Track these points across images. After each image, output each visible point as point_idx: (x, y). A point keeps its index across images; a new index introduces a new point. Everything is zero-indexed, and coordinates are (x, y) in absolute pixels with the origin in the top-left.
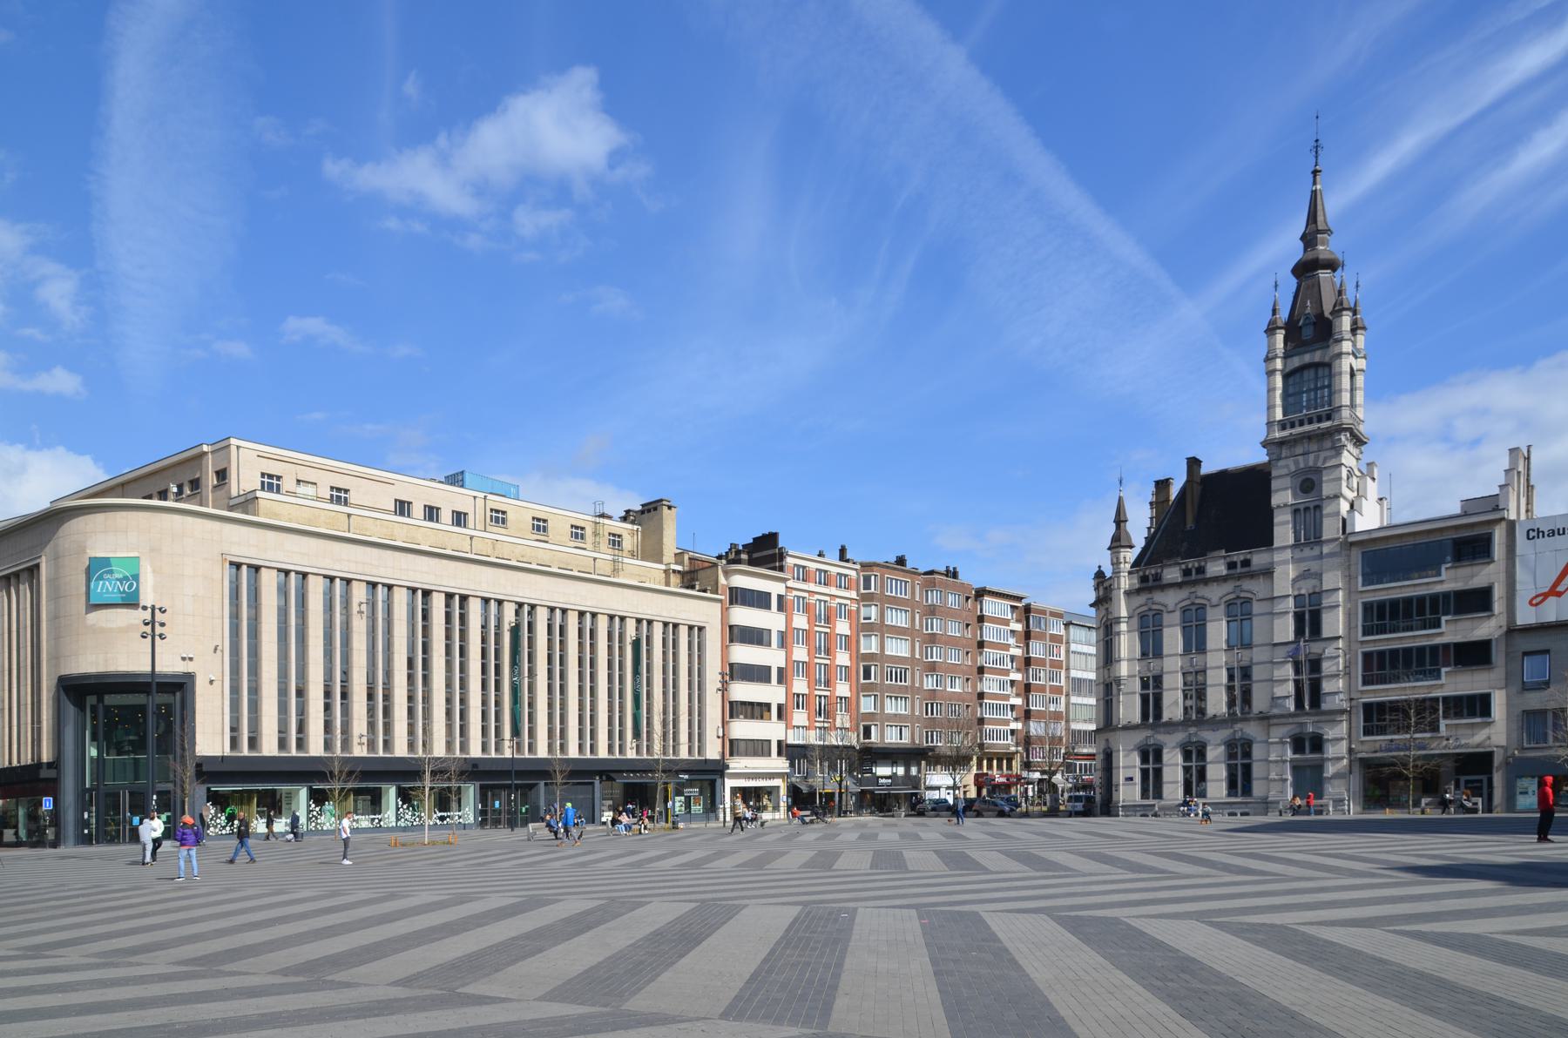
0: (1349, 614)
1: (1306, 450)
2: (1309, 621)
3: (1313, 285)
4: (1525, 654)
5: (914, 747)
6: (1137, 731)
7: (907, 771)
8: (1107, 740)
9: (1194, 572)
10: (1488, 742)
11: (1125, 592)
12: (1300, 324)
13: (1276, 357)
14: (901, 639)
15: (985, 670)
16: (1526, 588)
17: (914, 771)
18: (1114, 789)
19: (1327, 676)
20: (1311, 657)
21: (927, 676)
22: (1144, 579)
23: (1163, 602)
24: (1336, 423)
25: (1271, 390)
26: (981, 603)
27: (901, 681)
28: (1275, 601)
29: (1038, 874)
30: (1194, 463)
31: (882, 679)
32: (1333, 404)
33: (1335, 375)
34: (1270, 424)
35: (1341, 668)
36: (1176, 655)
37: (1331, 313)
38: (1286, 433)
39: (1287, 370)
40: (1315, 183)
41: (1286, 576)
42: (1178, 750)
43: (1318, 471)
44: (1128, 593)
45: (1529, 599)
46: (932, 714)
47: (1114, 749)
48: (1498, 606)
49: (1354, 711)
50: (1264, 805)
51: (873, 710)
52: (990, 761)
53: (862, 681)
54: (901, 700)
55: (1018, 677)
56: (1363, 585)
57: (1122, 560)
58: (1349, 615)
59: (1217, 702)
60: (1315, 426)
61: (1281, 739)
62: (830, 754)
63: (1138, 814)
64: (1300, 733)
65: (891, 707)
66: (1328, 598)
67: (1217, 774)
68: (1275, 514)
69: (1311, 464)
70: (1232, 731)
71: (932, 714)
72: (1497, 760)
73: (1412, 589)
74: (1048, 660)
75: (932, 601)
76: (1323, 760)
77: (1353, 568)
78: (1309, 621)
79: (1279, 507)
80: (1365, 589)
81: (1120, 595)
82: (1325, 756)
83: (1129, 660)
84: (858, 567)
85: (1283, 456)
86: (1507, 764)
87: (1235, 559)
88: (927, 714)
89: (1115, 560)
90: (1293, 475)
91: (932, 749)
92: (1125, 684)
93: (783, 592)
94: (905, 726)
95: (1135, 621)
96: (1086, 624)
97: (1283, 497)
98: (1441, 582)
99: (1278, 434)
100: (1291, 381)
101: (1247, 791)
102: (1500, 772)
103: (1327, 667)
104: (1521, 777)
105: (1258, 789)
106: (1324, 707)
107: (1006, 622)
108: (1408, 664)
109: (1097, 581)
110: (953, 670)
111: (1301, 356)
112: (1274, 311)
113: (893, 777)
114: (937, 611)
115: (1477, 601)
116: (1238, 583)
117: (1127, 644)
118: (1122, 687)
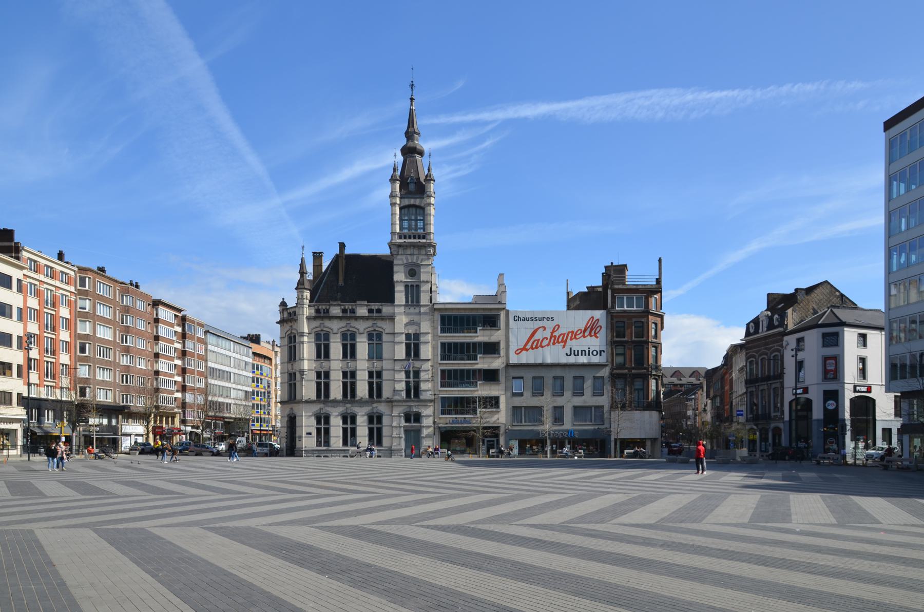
0: (434, 348)
1: (412, 252)
2: (413, 349)
3: (413, 162)
4: (514, 378)
5: (115, 405)
6: (314, 404)
7: (110, 422)
8: (292, 409)
9: (349, 312)
10: (498, 421)
11: (307, 317)
12: (409, 181)
13: (396, 196)
14: (104, 326)
15: (160, 355)
16: (513, 347)
17: (114, 422)
18: (297, 439)
19: (423, 381)
20: (415, 369)
21: (123, 355)
22: (318, 311)
23: (330, 327)
24: (428, 241)
25: (393, 214)
26: (157, 310)
27: (107, 357)
28: (396, 335)
29: (83, 497)
30: (342, 246)
31: (94, 354)
32: (426, 230)
33: (427, 215)
34: (393, 233)
35: (430, 376)
36: (338, 360)
37: (425, 181)
38: (402, 241)
39: (402, 205)
40: (411, 105)
41: (401, 322)
42: (340, 417)
43: (419, 266)
44: (308, 318)
45: (515, 350)
46: (127, 382)
47: (297, 414)
48: (503, 352)
49: (436, 401)
50: (390, 452)
51: (87, 376)
52: (161, 417)
53: (79, 354)
54: (107, 370)
55: (179, 362)
56: (441, 333)
57: (305, 297)
58: (434, 348)
59: (362, 390)
60: (417, 240)
61: (399, 414)
62: (58, 407)
63: (315, 455)
64: (409, 411)
65: (99, 377)
66: (397, 337)
67: (362, 432)
68: (395, 286)
69: (415, 261)
70: (371, 408)
71: (127, 382)
72: (502, 431)
73: (464, 338)
74: (196, 354)
75: (127, 303)
76: (421, 427)
77: (435, 322)
78: (413, 349)
79: (397, 282)
80: (441, 335)
81: (304, 318)
82: (422, 425)
83: (308, 360)
84: (76, 269)
85: (400, 253)
86: (506, 432)
87: (373, 308)
88: (123, 382)
89: (300, 297)
90: (406, 265)
91: (128, 407)
92: (306, 375)
93: (21, 278)
94: (110, 390)
95: (313, 335)
96: (217, 334)
97: (399, 276)
98: (477, 336)
99: (398, 240)
100: (403, 210)
101: (379, 443)
102: (503, 437)
103: (423, 376)
104: (511, 440)
105: (386, 442)
106: (422, 397)
107: (172, 325)
108: (462, 378)
109: (282, 308)
110: (140, 352)
111: (409, 199)
112: (395, 170)
113: (100, 425)
114: (130, 311)
115: (492, 349)
116: (375, 322)
117: (307, 349)
118: (304, 376)
